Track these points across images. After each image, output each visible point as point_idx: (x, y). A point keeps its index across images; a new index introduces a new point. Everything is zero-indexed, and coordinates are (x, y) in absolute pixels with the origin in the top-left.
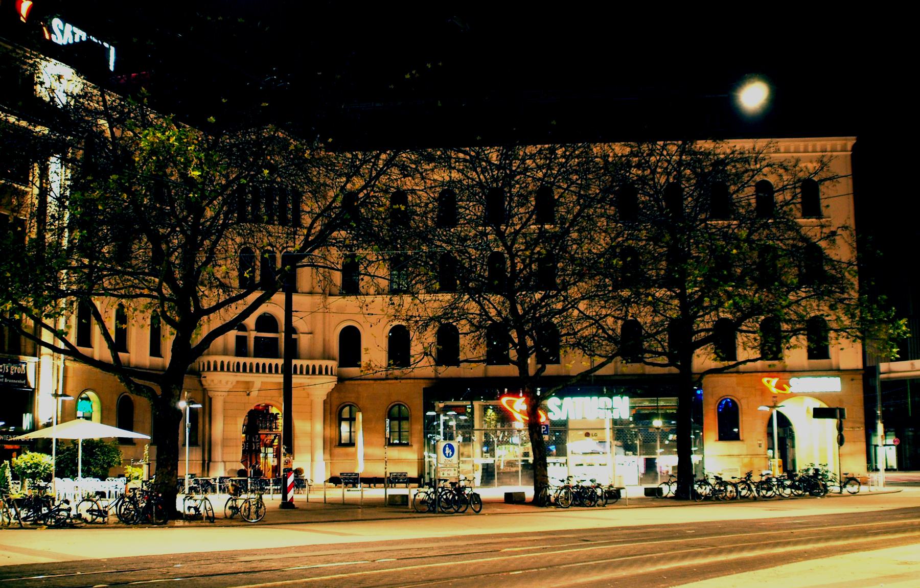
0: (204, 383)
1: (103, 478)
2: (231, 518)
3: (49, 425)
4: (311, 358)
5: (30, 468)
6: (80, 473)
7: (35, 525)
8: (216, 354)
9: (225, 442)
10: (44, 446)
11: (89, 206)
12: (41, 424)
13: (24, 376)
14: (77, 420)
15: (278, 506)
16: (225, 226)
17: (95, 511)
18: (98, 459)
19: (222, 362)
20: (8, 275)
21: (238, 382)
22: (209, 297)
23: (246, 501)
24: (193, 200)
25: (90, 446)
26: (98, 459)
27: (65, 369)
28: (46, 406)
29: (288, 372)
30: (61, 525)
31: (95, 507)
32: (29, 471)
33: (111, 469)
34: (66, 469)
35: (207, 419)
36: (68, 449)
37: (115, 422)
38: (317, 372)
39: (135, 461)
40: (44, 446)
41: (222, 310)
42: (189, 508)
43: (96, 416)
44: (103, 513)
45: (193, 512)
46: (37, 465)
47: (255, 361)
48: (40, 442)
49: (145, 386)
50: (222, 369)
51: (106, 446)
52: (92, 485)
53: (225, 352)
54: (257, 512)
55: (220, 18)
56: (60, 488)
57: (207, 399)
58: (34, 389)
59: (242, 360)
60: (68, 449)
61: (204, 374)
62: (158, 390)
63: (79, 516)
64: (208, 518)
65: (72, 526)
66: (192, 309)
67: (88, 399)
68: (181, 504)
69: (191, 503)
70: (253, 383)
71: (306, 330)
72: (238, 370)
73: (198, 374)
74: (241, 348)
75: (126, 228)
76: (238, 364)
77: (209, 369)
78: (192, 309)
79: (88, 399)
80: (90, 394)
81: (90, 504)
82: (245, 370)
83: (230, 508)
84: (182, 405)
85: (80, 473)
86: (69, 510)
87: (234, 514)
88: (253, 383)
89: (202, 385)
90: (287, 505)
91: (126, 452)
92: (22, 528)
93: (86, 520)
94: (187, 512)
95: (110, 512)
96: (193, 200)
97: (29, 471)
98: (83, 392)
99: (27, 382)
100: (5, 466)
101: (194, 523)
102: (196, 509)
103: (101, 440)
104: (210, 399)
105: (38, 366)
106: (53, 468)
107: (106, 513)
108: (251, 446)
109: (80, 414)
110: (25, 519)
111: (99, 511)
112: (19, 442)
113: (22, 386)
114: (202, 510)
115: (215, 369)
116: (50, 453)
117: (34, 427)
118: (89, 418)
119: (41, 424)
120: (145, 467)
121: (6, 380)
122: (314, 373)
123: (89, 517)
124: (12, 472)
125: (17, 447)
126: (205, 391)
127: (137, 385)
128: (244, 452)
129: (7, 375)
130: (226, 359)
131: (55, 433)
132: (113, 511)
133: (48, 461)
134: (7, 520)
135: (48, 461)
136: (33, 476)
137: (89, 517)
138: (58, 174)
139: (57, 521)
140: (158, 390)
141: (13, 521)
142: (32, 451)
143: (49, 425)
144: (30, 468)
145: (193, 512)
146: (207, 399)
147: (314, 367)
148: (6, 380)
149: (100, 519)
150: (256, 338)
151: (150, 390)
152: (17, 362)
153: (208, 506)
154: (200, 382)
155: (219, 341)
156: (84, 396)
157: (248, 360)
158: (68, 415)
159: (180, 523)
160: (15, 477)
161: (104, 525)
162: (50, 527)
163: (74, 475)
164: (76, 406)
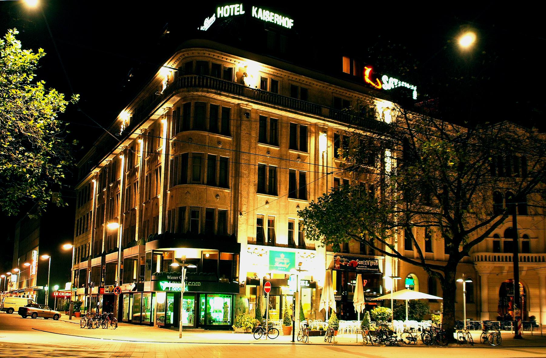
0: (476, 268)
1: (419, 321)
2: (484, 343)
3: (390, 292)
4: (537, 252)
5: (380, 315)
6: (407, 318)
7: (380, 344)
8: (482, 252)
9: (489, 302)
10: (385, 303)
11: (409, 176)
12: (387, 291)
13: (377, 267)
14: (405, 290)
15: (512, 337)
16: (477, 184)
17: (410, 338)
18: (417, 310)
19: (486, 256)
20: (363, 219)
21: (495, 267)
22: (470, 221)
23: (492, 334)
24: (224, 276)
25: (413, 303)
26: (417, 310)
27: (399, 262)
28: (389, 283)
29: (516, 261)
30: (392, 344)
31: (410, 336)
32: (379, 317)
33: (424, 316)
34: (399, 315)
35: (478, 288)
36: (401, 305)
37: (426, 291)
38: (541, 260)
39: (436, 312)
40: (385, 303)
41: (478, 229)
42: (460, 337)
43: (416, 287)
44: (414, 339)
45: (462, 339)
46: (384, 313)
47: (504, 255)
48: (387, 301)
49: (437, 273)
50: (486, 260)
51: (421, 304)
52: (414, 324)
53: (487, 250)
54: (497, 340)
55: (462, 78)
56: (397, 326)
57: (478, 277)
58: (383, 274)
59: (497, 254)
60: (401, 305)
61: (476, 263)
62: (442, 273)
63: (402, 340)
64: (470, 343)
65: (398, 345)
66: (459, 231)
67: (411, 278)
68: (457, 335)
69: (461, 335)
70: (504, 267)
71: (534, 236)
72: (495, 260)
73: (471, 262)
74: (496, 247)
75: (427, 187)
76: (495, 257)
77: (478, 260)
78: (459, 231)
79: (411, 278)
80: (413, 275)
81: (408, 334)
82: (499, 260)
83: (483, 338)
84: (460, 280)
85: (407, 318)
86: (396, 337)
87: (485, 341)
88: (504, 267)
89: (475, 269)
90: (518, 336)
91: (432, 306)
92: (373, 345)
93: (405, 342)
94: (459, 340)
95: (418, 339)
96: (224, 276)
97: (379, 317)
98: (409, 274)
99: (379, 270)
100: (367, 314)
101: (462, 345)
102: (464, 338)
103: (419, 300)
104: (480, 277)
105: (384, 261)
106: (392, 315)
107: (416, 339)
108: (503, 303)
109: (407, 286)
110: (375, 341)
111: (412, 338)
112: (376, 301)
113: (376, 272)
114: (467, 338)
115: (482, 260)
116: (390, 308)
117: (384, 294)
118: (412, 288)
119: (387, 291)
120: (441, 315)
121: (368, 269)
122: (539, 261)
123: (407, 341)
124: (371, 317)
125: (376, 304)
126: (476, 272)
127: (433, 272)
128: (499, 306)
129: (369, 266)
130: (488, 254)
131: (392, 297)
132: (419, 338)
133: (389, 311)
134: (366, 342)
135: (389, 311)
136: (382, 319)
137: (407, 341)
138: (390, 162)
139: (391, 342)
140: (442, 273)
141: (369, 342)
142: (381, 306)
143: (390, 292)
144: (380, 315)
145: (462, 339)
146: (478, 277)
147: (539, 257)
148: (368, 269)
149: (413, 342)
150: (505, 242)
151: (439, 274)
152: (373, 259)
153: (470, 336)
154: (474, 267)
155: (483, 243)
156: (409, 276)
157: (500, 254)
158: (401, 287)
159: (456, 345)
160: (372, 320)
161: (415, 345)
162: (387, 346)
163: (404, 319)
164: (405, 281)
